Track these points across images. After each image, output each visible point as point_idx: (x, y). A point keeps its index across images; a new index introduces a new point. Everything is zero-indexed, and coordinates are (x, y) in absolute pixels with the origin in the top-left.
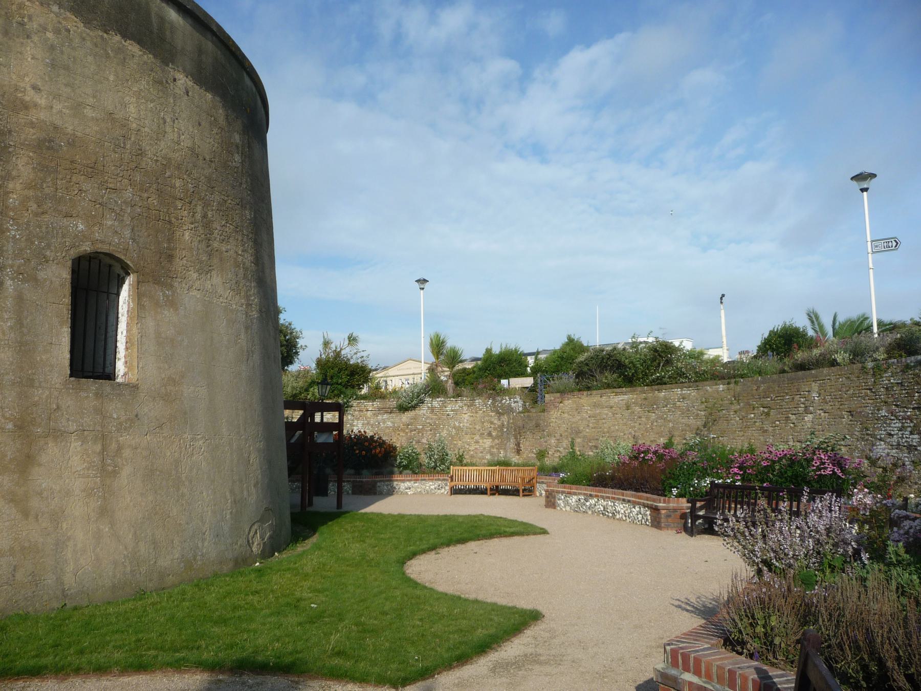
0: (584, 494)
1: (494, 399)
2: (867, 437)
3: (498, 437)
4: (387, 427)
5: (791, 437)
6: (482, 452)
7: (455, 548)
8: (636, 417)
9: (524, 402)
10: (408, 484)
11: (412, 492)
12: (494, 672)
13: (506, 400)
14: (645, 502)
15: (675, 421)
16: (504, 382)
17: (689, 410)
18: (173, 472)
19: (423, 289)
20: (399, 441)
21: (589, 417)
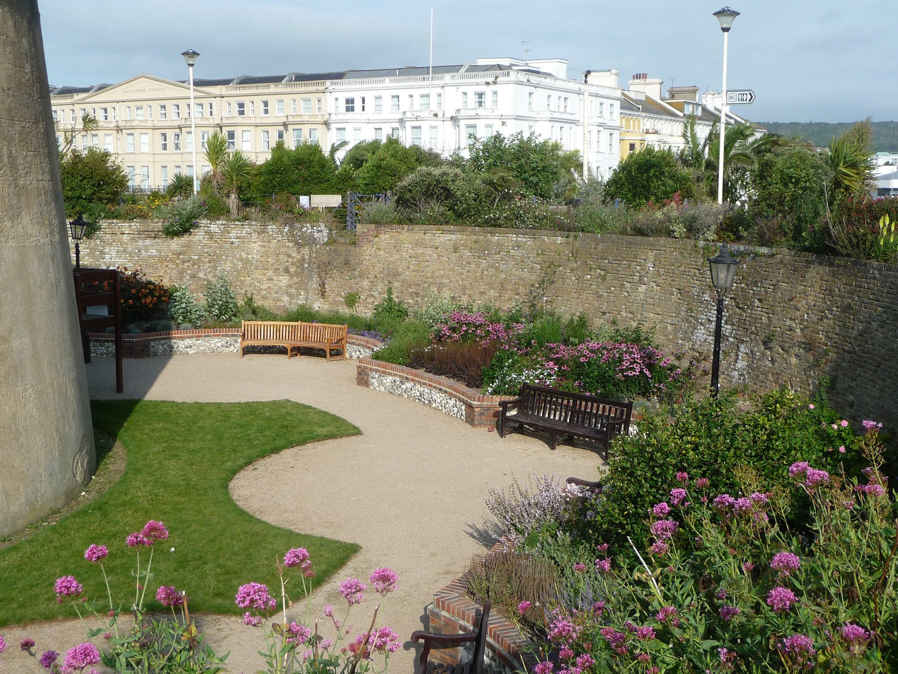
0: (400, 376)
1: (292, 226)
2: (691, 319)
3: (296, 274)
4: (150, 257)
5: (624, 307)
6: (276, 293)
7: (270, 459)
8: (464, 263)
9: (330, 230)
10: (188, 342)
11: (193, 352)
12: (329, 601)
13: (307, 228)
14: (461, 396)
15: (507, 272)
16: (304, 200)
17: (523, 261)
18: (13, 426)
19: (192, 65)
20: (164, 276)
21: (410, 257)
